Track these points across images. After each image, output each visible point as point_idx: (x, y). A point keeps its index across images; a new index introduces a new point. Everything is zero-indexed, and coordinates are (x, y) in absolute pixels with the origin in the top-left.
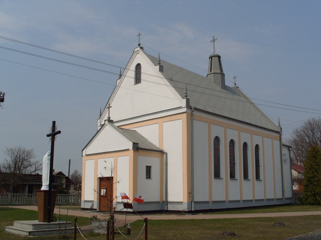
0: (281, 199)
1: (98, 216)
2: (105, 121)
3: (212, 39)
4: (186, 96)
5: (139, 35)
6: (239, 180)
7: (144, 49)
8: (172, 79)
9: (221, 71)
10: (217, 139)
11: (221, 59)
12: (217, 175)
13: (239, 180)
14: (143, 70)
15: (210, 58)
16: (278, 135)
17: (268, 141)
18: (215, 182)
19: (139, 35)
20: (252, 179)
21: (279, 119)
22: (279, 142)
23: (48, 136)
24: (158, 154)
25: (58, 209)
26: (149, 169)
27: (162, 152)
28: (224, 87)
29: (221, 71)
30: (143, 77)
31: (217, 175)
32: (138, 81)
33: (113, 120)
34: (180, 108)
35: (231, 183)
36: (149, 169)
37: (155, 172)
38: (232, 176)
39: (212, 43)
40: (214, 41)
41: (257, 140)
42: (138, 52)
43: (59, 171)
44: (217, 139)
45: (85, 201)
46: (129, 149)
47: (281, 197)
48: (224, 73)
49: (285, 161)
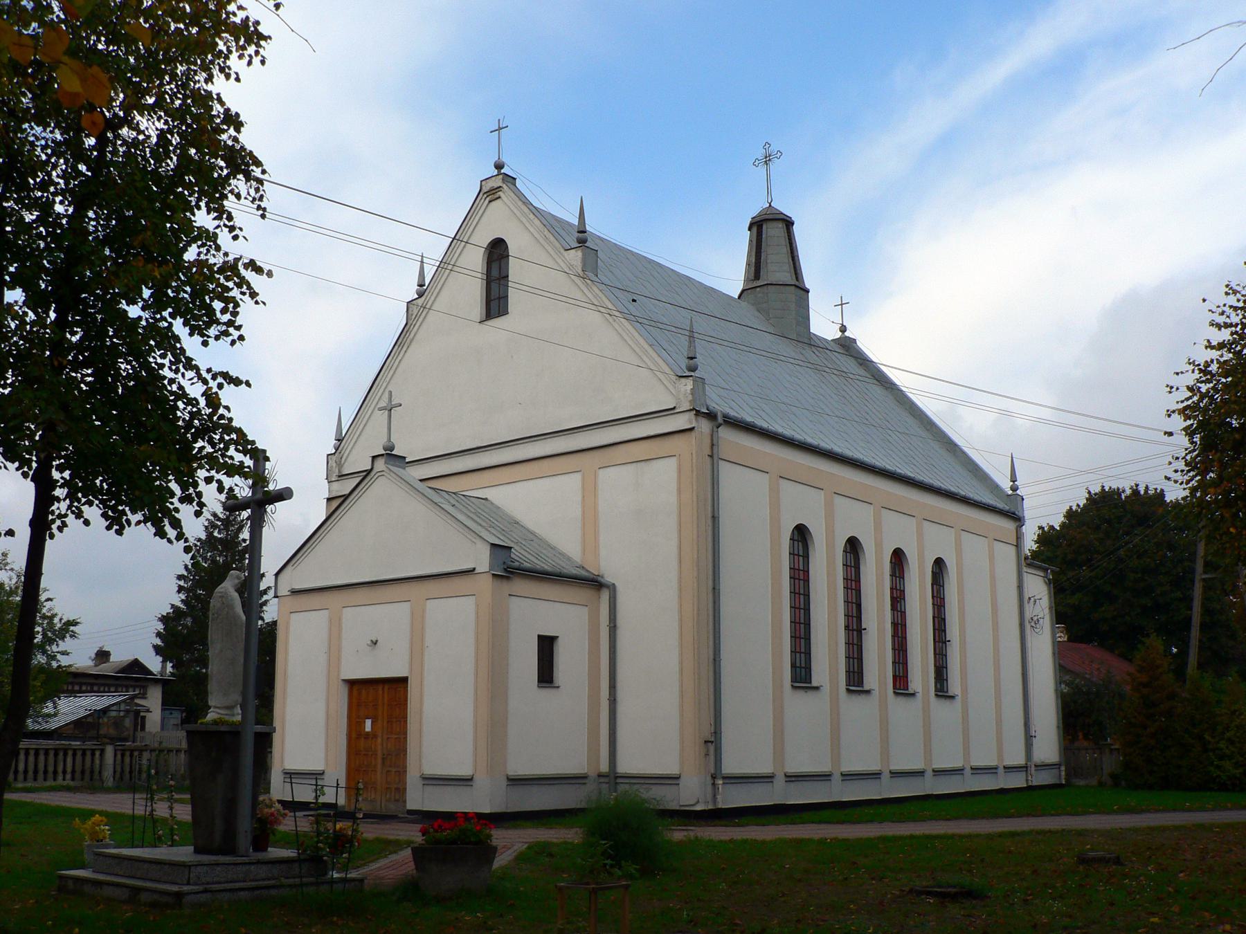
0: (1024, 768)
1: (417, 836)
2: (374, 458)
3: (760, 153)
4: (693, 369)
5: (500, 129)
6: (826, 689)
7: (518, 183)
8: (634, 301)
9: (797, 279)
10: (801, 534)
11: (796, 229)
12: (802, 676)
13: (876, 693)
14: (515, 270)
15: (755, 229)
16: (1009, 525)
17: (975, 548)
18: (799, 704)
19: (500, 129)
20: (877, 689)
21: (1012, 457)
22: (1012, 550)
23: (283, 495)
24: (583, 594)
25: (167, 805)
26: (547, 645)
27: (595, 584)
28: (334, 454)
29: (797, 279)
30: (515, 297)
31: (802, 676)
32: (494, 304)
33: (405, 458)
34: (670, 411)
35: (899, 707)
36: (547, 645)
37: (567, 661)
38: (855, 679)
39: (762, 170)
40: (767, 160)
41: (939, 543)
42: (497, 196)
43: (132, 658)
44: (801, 534)
45: (290, 775)
46: (474, 569)
47: (1020, 760)
48: (807, 286)
49: (1033, 624)
